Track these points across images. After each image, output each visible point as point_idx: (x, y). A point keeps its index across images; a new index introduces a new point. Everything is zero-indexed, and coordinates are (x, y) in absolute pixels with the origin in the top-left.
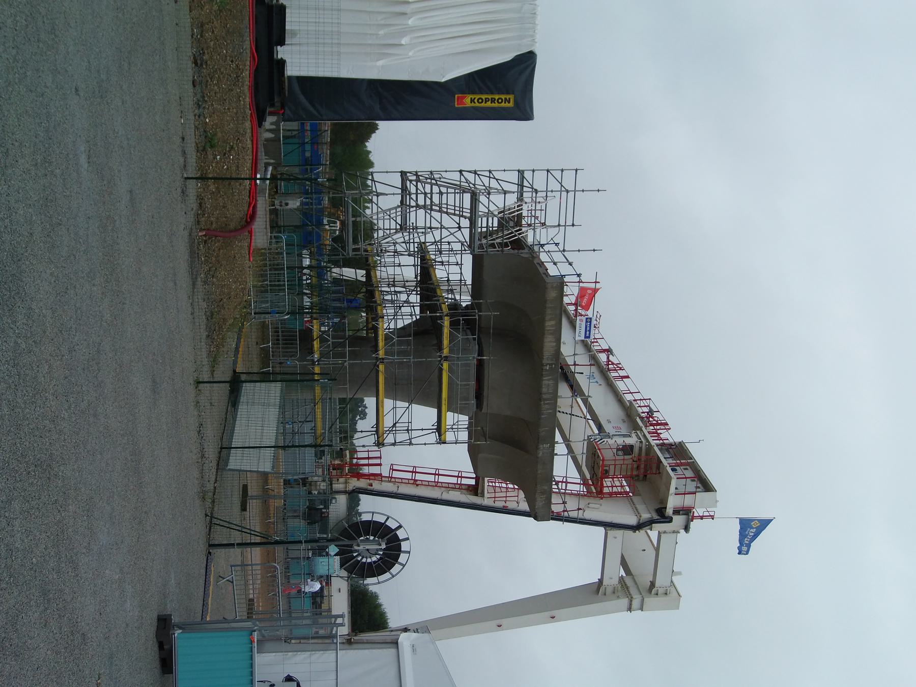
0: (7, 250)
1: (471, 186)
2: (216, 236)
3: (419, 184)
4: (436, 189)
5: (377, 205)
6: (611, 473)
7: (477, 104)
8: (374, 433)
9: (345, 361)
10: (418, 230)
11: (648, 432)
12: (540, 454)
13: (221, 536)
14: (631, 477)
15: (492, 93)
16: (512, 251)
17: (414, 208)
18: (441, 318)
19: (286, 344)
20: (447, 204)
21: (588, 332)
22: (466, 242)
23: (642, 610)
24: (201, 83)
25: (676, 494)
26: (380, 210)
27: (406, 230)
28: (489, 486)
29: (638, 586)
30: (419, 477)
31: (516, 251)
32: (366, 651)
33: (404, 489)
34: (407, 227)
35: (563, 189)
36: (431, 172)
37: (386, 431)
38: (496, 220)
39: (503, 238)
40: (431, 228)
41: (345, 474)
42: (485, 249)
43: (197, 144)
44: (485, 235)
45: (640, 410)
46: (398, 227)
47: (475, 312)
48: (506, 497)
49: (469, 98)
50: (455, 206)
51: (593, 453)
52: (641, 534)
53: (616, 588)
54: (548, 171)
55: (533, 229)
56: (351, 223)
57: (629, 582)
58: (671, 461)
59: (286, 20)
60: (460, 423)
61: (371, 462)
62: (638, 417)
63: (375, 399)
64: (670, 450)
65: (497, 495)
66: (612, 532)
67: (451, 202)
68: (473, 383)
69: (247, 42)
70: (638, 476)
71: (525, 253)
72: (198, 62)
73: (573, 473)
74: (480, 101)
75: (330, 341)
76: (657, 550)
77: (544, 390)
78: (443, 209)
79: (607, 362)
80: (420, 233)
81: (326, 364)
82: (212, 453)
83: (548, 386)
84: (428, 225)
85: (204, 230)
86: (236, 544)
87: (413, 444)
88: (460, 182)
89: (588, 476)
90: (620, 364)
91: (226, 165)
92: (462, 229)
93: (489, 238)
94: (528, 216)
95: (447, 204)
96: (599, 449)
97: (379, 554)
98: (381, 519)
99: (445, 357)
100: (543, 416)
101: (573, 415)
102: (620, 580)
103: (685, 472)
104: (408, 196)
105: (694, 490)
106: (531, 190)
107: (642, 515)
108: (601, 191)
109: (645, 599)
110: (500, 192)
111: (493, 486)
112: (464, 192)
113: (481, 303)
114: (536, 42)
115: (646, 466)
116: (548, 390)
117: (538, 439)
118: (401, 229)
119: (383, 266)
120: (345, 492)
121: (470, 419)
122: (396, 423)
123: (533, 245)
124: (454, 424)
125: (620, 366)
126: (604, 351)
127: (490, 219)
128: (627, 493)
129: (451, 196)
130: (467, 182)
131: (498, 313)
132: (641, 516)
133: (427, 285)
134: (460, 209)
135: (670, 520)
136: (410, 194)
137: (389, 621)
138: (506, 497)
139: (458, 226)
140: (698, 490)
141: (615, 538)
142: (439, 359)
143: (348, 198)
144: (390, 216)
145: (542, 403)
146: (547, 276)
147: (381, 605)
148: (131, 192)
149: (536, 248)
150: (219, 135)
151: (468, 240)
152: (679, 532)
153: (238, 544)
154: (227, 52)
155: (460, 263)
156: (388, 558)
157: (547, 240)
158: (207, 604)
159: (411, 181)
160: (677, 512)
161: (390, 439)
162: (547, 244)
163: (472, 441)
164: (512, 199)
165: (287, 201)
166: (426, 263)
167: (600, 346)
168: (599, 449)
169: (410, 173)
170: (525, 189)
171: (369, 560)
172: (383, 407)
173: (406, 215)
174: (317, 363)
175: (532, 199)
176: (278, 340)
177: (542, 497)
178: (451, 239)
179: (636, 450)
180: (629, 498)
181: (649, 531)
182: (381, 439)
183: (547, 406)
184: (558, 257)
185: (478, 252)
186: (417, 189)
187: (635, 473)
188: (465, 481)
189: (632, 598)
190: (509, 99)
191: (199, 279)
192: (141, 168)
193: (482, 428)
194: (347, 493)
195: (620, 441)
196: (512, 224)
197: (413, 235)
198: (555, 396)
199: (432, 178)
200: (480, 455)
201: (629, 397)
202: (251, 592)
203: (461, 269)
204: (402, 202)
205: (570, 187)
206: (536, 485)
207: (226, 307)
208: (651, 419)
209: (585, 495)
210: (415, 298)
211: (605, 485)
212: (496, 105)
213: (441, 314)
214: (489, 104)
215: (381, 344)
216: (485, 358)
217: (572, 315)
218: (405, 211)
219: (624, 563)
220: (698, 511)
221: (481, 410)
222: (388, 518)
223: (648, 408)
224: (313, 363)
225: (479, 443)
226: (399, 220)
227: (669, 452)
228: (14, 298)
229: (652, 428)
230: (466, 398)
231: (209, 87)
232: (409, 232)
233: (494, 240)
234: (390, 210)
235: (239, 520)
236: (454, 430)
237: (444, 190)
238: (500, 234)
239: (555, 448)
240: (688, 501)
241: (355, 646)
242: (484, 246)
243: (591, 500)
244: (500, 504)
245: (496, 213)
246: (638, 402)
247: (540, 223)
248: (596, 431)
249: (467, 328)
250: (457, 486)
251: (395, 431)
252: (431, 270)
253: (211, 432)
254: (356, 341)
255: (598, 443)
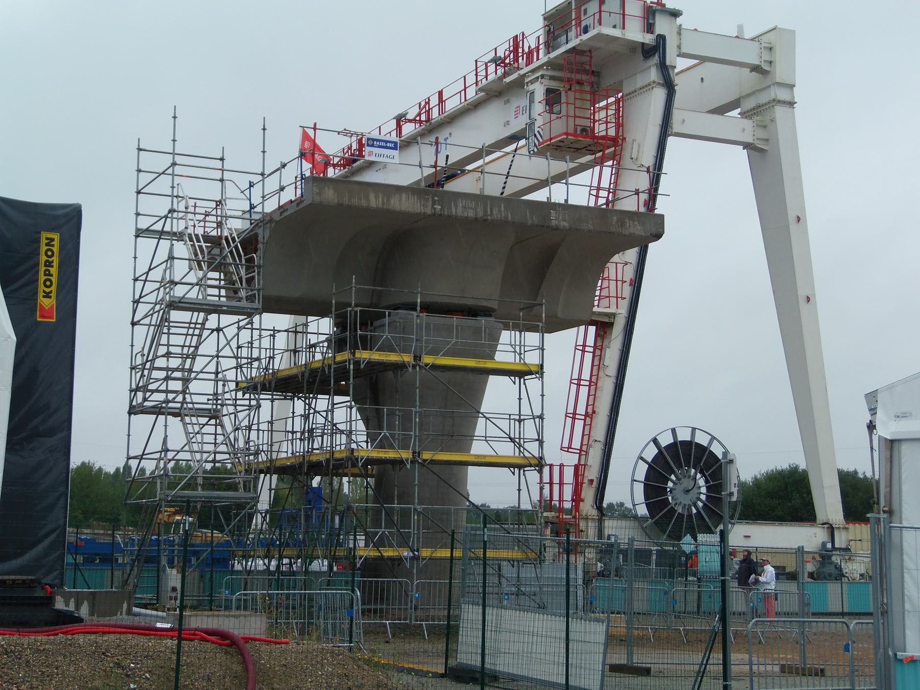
3: (150, 387)
4: (161, 362)
5: (178, 452)
6: (587, 123)
7: (54, 288)
8: (522, 471)
9: (415, 509)
10: (220, 391)
11: (527, 66)
12: (564, 224)
14: (594, 95)
15: (37, 264)
17: (187, 396)
18: (357, 363)
19: (382, 599)
21: (388, 145)
22: (238, 322)
23: (794, 86)
25: (624, 28)
26: (187, 448)
27: (219, 411)
28: (598, 307)
29: (757, 91)
30: (581, 410)
31: (260, 246)
32: (905, 488)
33: (599, 432)
34: (214, 409)
35: (170, 171)
36: (132, 368)
37: (520, 451)
39: (238, 265)
40: (217, 373)
41: (573, 520)
42: (256, 292)
44: (233, 292)
45: (491, 77)
46: (213, 422)
47: (350, 311)
48: (617, 281)
49: (42, 299)
50: (187, 335)
52: (680, 83)
53: (759, 123)
54: (139, 192)
55: (226, 220)
56: (206, 493)
57: (749, 104)
58: (572, 34)
60: (513, 343)
61: (556, 479)
62: (504, 80)
63: (471, 469)
64: (556, 34)
65: (613, 293)
67: (180, 340)
68: (455, 320)
70: (591, 84)
71: (263, 234)
73: (585, 177)
75: (384, 532)
76: (703, 59)
77: (471, 214)
78: (190, 352)
79: (415, 123)
80: (224, 389)
81: (418, 538)
83: (465, 207)
86: (725, 683)
87: (542, 414)
88: (150, 325)
89: (589, 158)
90: (420, 103)
91: (144, 675)
92: (221, 326)
93: (238, 285)
94: (205, 227)
95: (183, 347)
96: (551, 139)
98: (643, 469)
99: (415, 360)
100: (510, 218)
101: (508, 173)
103: (590, 13)
104: (171, 405)
106: (169, 220)
107: (652, 80)
108: (175, 113)
110: (171, 266)
111: (599, 300)
112: (167, 320)
113: (336, 302)
115: (577, 72)
116: (471, 208)
117: (543, 226)
118: (216, 418)
119: (271, 448)
120: (600, 521)
121: (507, 328)
122: (510, 438)
123: (251, 220)
124: (515, 352)
125: (423, 104)
126: (399, 127)
127: (210, 282)
128: (617, 101)
129: (174, 340)
130: (152, 315)
131: (354, 276)
132: (654, 82)
133: (305, 382)
134: (192, 328)
135: (661, 39)
136: (167, 401)
137: (779, 468)
139: (215, 332)
141: (684, 121)
142: (418, 368)
143: (168, 496)
144: (198, 433)
145: (489, 218)
146: (301, 202)
147: (756, 478)
149: (256, 217)
151: (235, 318)
152: (680, 25)
153: (725, 679)
155: (272, 333)
156: (701, 460)
157: (243, 199)
159: (145, 399)
160: (650, 28)
161: (533, 448)
162: (250, 200)
163: (541, 325)
164: (182, 250)
165: (169, 589)
166: (270, 383)
167: (390, 133)
168: (551, 139)
169: (131, 401)
170: (167, 228)
171: (704, 490)
173: (197, 409)
174: (416, 553)
175: (181, 218)
176: (375, 611)
177: (628, 224)
179: (554, 85)
180: (624, 98)
181: (676, 71)
183: (494, 213)
184: (272, 184)
185: (259, 302)
186: (157, 391)
187: (587, 88)
188: (591, 341)
189: (774, 100)
190: (47, 239)
193: (522, 309)
194: (601, 518)
195: (539, 107)
196: (216, 251)
197: (226, 399)
198: (480, 199)
200: (560, 315)
201: (471, 93)
202: (769, 668)
203: (279, 331)
204: (175, 415)
205: (169, 159)
206: (610, 233)
207: (360, 681)
208: (507, 61)
209: (619, 163)
210: (322, 402)
211: (604, 133)
212: (55, 260)
213: (352, 362)
214: (54, 271)
215: (391, 454)
216: (419, 300)
217: (341, 172)
218: (191, 411)
219: (721, 110)
221: (494, 310)
222: (642, 459)
223: (489, 64)
224: (415, 558)
225: (544, 316)
226: (203, 420)
227: (559, 36)
229: (520, 59)
230: (477, 331)
232: (222, 405)
233: (241, 279)
234: (187, 433)
235: (667, 680)
236: (522, 352)
237: (162, 350)
238: (232, 269)
239: (557, 202)
241: (895, 506)
242: (250, 293)
243: (626, 155)
244: (627, 291)
245: (201, 274)
246: (479, 78)
247: (216, 208)
249: (372, 324)
250: (598, 352)
251: (520, 439)
252: (280, 375)
254: (382, 492)
255: (541, 141)
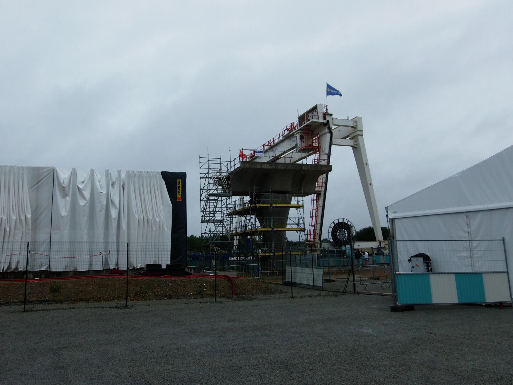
0: (271, 366)
1: (206, 196)
2: (235, 291)
3: (206, 216)
5: (213, 231)
6: (311, 143)
7: (181, 193)
13: (350, 289)
16: (231, 181)
17: (215, 218)
18: (256, 207)
20: (213, 205)
22: (226, 198)
23: (362, 131)
24: (177, 296)
26: (215, 230)
30: (314, 215)
31: (231, 179)
33: (319, 221)
35: (207, 162)
38: (219, 187)
43: (201, 298)
45: (286, 134)
46: (221, 224)
48: (321, 182)
50: (214, 202)
51: (303, 150)
52: (334, 132)
54: (200, 168)
56: (220, 241)
57: (352, 136)
58: (305, 122)
59: (150, 264)
61: (309, 233)
63: (286, 232)
66: (333, 142)
69: (162, 279)
70: (311, 134)
71: (231, 176)
72: (170, 297)
73: (311, 157)
74: (179, 192)
76: (339, 126)
77: (283, 168)
82: (317, 293)
84: (221, 212)
85: (233, 295)
87: (304, 217)
89: (312, 152)
96: (302, 148)
97: (344, 230)
98: (331, 230)
100: (292, 168)
102: (351, 139)
103: (310, 116)
104: (211, 220)
105: (316, 113)
106: (208, 174)
109: (359, 129)
110: (209, 185)
114: (158, 171)
115: (308, 131)
118: (222, 223)
124: (296, 202)
125: (269, 141)
126: (264, 147)
127: (219, 189)
132: (327, 132)
135: (328, 121)
136: (210, 219)
137: (366, 227)
138: (321, 182)
140: (316, 111)
148: (228, 321)
150: (197, 289)
154: (165, 286)
158: (378, 294)
159: (205, 219)
160: (325, 119)
161: (302, 226)
163: (302, 195)
164: (211, 181)
165: (213, 266)
168: (302, 148)
169: (201, 220)
170: (208, 176)
171: (347, 234)
172: (290, 229)
178: (225, 204)
179: (302, 134)
181: (333, 129)
182: (302, 229)
184: (233, 164)
186: (207, 217)
187: (310, 135)
191: (252, 297)
192: (217, 317)
193: (297, 191)
195: (298, 140)
199: (203, 211)
204: (212, 222)
208: (290, 129)
210: (248, 217)
211: (315, 146)
212: (181, 186)
214: (180, 188)
215: (266, 229)
216: (271, 190)
219: (345, 138)
220: (325, 111)
226: (219, 223)
227: (302, 122)
228: (289, 364)
231: (179, 293)
232: (224, 219)
233: (226, 188)
234: (215, 227)
237: (208, 207)
238: (224, 185)
240: (321, 115)
241: (394, 235)
243: (321, 150)
244: (324, 185)
245: (216, 187)
246: (283, 134)
248: (295, 149)
250: (317, 201)
253: (310, 293)
